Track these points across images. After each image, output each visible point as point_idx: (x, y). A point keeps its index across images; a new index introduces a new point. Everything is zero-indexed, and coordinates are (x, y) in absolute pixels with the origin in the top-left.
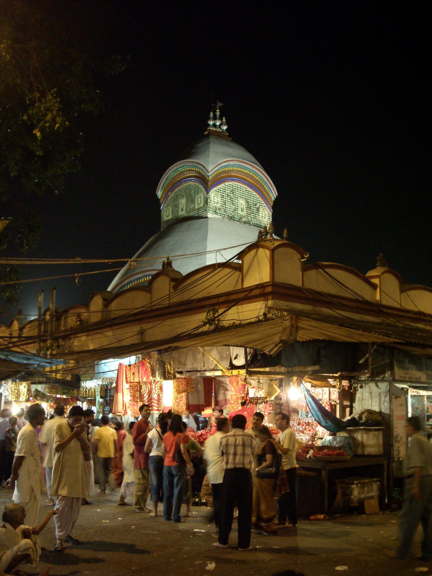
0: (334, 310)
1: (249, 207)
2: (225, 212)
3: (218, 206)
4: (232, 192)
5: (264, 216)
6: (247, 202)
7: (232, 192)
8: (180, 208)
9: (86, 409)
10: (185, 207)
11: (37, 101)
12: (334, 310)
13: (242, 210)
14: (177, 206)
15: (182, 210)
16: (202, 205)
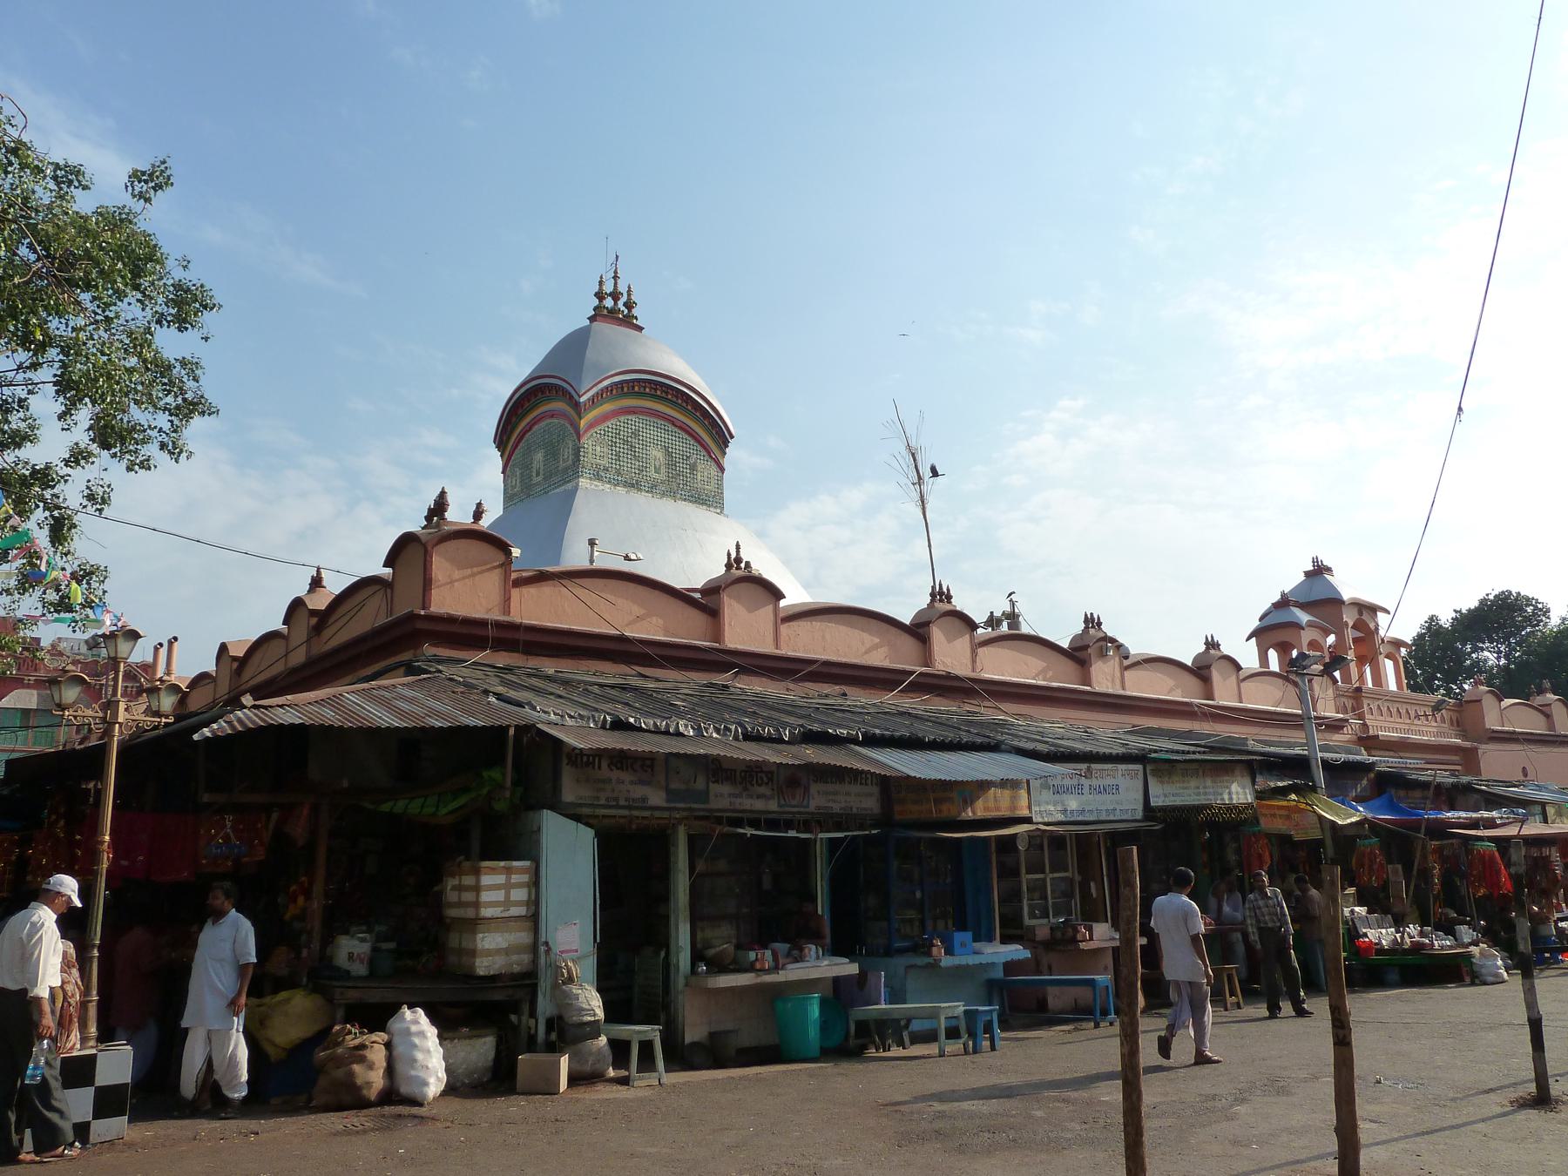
1: (671, 464)
3: (604, 462)
6: (669, 454)
7: (635, 434)
13: (657, 471)
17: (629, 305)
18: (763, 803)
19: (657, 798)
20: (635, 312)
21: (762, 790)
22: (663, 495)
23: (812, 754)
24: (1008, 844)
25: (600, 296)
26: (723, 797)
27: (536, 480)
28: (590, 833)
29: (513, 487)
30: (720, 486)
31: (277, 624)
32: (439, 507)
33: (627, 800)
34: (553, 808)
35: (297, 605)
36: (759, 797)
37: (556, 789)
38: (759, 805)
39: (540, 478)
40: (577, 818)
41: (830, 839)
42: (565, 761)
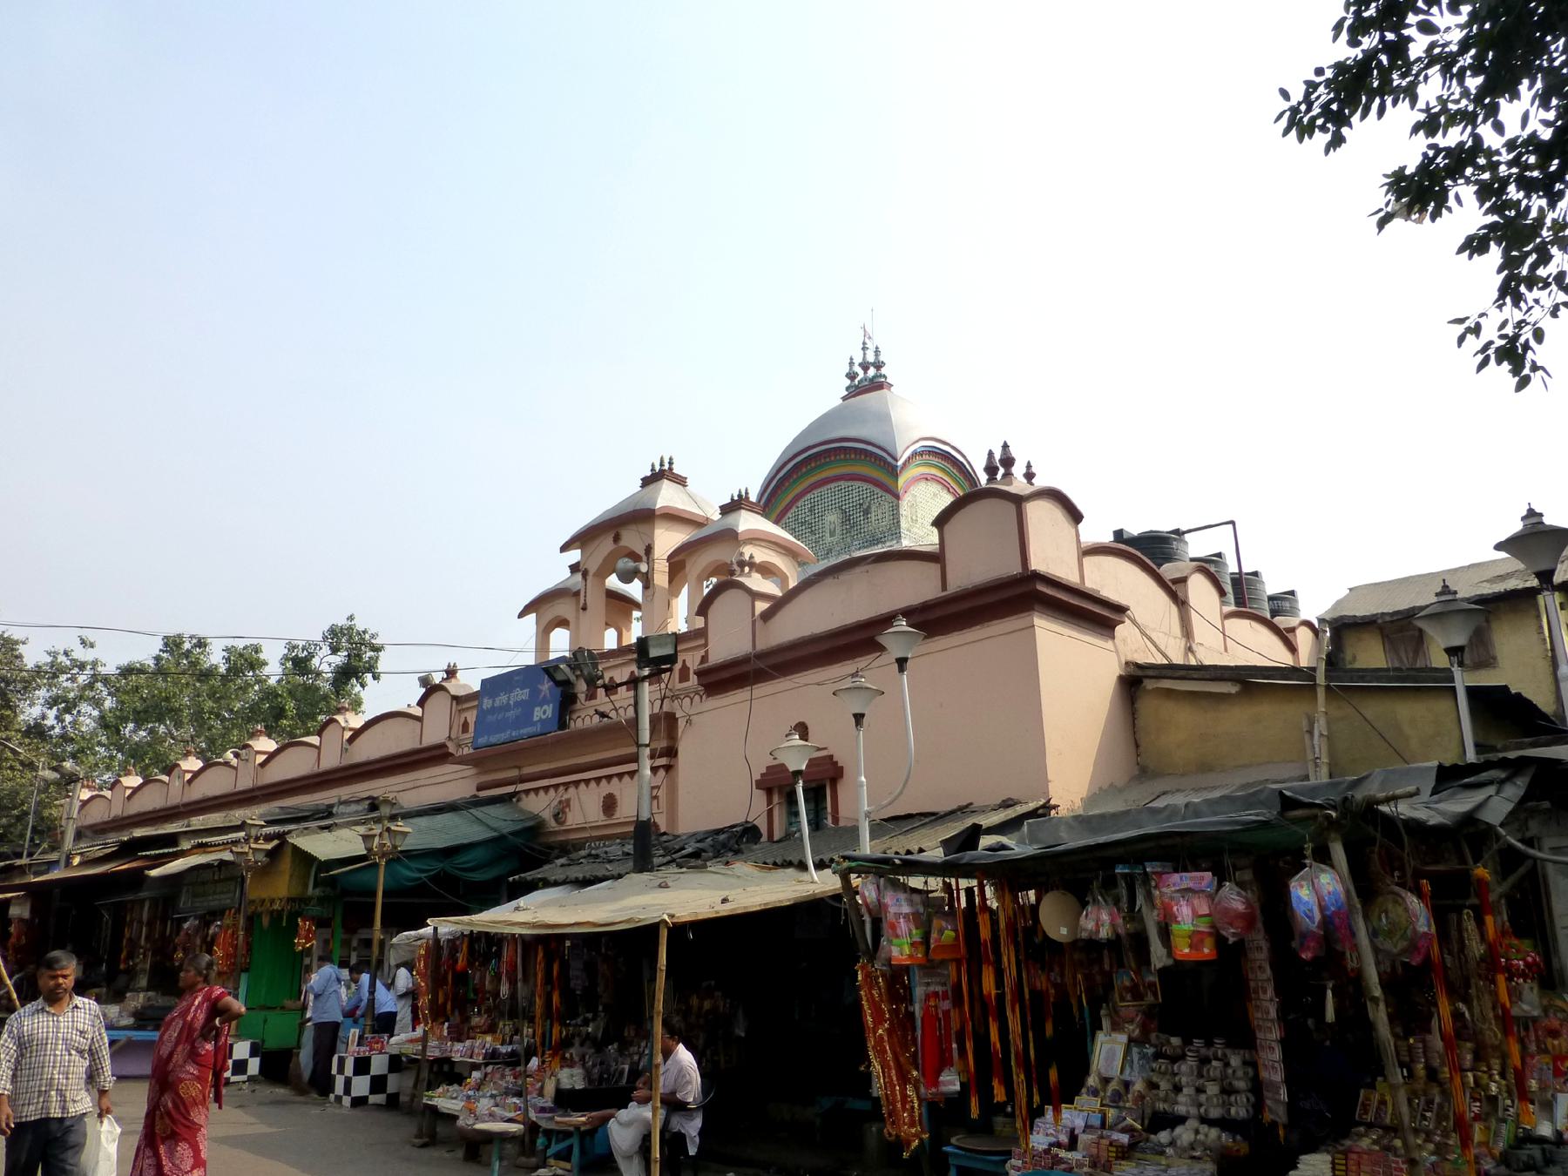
20: (883, 371)
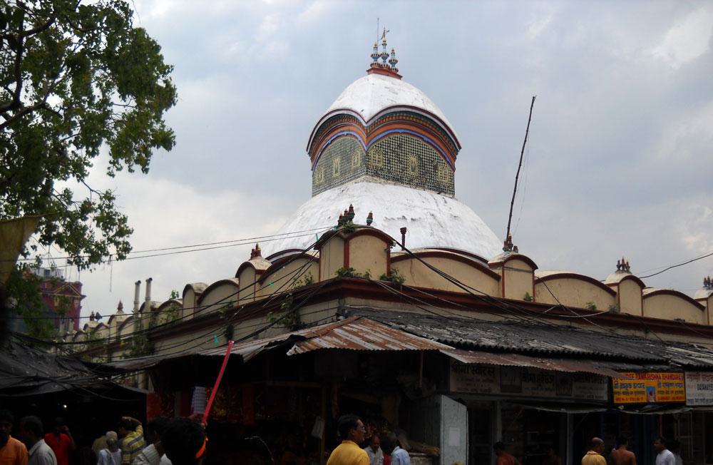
0: (466, 292)
1: (422, 166)
2: (390, 172)
3: (380, 165)
4: (400, 146)
5: (443, 175)
6: (420, 159)
7: (400, 146)
8: (334, 169)
9: (334, 276)
10: (339, 168)
11: (521, 412)
12: (466, 292)
13: (413, 170)
14: (330, 166)
15: (336, 172)
16: (359, 165)
17: (394, 62)
18: (548, 393)
19: (496, 390)
20: (397, 66)
21: (550, 386)
22: (417, 186)
23: (671, 381)
24: (669, 419)
25: (375, 57)
26: (528, 390)
27: (335, 175)
28: (463, 409)
29: (319, 180)
30: (452, 179)
31: (231, 275)
32: (350, 214)
33: (481, 390)
34: (445, 394)
35: (245, 267)
36: (547, 390)
37: (446, 384)
38: (547, 394)
39: (338, 174)
40: (460, 401)
41: (574, 414)
42: (451, 368)
